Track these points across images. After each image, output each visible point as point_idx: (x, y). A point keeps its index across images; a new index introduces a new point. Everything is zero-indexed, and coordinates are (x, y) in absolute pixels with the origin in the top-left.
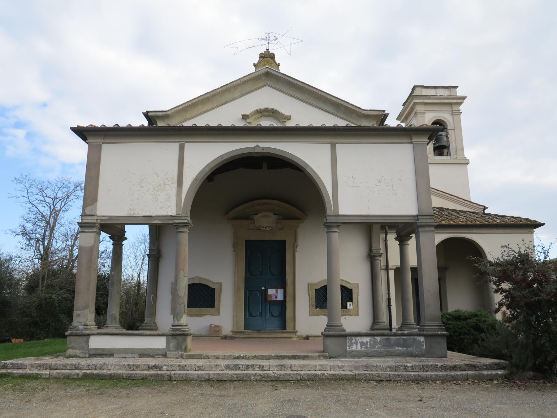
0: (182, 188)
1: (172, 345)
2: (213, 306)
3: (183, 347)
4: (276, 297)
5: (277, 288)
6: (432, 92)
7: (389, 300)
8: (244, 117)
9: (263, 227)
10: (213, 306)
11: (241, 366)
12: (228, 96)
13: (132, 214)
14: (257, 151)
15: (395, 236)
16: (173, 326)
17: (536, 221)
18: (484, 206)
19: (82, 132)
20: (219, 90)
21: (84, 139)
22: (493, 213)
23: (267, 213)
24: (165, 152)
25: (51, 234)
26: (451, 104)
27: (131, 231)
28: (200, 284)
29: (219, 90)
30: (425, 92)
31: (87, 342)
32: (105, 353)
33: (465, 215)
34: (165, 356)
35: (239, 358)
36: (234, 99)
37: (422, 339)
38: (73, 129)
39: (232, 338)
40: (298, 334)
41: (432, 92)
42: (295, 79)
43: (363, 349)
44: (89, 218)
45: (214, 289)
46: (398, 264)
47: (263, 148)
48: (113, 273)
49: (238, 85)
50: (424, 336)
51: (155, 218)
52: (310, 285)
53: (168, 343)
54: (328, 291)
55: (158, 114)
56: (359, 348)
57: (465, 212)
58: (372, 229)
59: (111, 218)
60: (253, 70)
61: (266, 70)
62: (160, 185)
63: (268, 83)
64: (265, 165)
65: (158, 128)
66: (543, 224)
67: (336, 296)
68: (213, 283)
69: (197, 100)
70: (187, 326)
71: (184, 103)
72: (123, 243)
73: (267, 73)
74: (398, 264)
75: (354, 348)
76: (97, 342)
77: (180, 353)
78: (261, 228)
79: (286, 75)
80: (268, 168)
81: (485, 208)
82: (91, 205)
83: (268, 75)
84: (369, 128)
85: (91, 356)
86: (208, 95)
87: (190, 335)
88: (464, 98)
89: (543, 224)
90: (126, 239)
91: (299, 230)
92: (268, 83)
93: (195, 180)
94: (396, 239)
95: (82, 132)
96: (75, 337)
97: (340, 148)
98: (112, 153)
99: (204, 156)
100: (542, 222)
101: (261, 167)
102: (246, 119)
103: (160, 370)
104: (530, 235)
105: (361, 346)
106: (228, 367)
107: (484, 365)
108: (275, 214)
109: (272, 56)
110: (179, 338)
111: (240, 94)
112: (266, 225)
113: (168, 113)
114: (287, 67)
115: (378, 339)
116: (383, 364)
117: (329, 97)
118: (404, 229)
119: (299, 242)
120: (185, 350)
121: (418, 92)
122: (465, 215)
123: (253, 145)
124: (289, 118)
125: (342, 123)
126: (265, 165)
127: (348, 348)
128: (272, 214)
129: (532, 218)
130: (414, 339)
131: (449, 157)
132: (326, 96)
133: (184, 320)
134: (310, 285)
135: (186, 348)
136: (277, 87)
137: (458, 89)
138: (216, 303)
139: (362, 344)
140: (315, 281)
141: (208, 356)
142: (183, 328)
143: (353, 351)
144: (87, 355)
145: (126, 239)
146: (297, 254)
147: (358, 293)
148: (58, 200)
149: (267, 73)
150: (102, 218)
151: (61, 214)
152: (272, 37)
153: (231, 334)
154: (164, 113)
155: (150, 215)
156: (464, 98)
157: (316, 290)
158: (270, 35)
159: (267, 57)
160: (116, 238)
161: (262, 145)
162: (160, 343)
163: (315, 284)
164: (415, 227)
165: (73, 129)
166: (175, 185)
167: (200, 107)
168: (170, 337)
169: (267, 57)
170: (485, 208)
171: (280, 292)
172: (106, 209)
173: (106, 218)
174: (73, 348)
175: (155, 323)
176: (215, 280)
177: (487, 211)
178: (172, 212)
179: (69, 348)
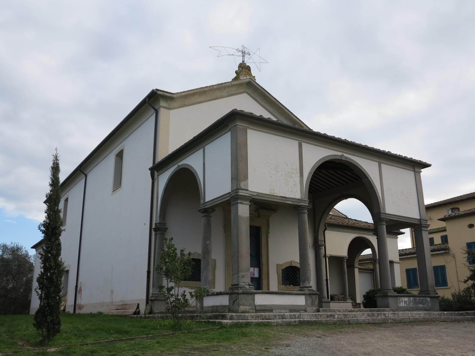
4: (254, 275)
12: (218, 93)
14: (343, 159)
20: (216, 87)
29: (216, 87)
31: (254, 300)
32: (267, 309)
36: (222, 97)
37: (429, 299)
42: (269, 94)
44: (244, 191)
47: (346, 158)
49: (228, 87)
50: (430, 297)
51: (289, 199)
52: (278, 265)
55: (166, 94)
56: (404, 305)
61: (250, 80)
62: (289, 173)
63: (248, 91)
69: (199, 90)
71: (188, 91)
79: (263, 89)
85: (257, 311)
86: (207, 89)
92: (248, 91)
93: (310, 173)
96: (244, 295)
104: (395, 238)
108: (255, 204)
110: (312, 296)
113: (175, 96)
115: (411, 298)
116: (421, 314)
117: (291, 115)
119: (271, 230)
123: (340, 154)
130: (426, 299)
132: (290, 113)
134: (278, 265)
136: (254, 96)
140: (281, 263)
141: (334, 310)
143: (401, 307)
146: (269, 239)
149: (244, 80)
152: (246, 51)
154: (171, 95)
155: (285, 196)
158: (245, 49)
159: (244, 69)
161: (346, 155)
163: (280, 265)
166: (298, 175)
167: (197, 97)
168: (308, 296)
169: (244, 69)
173: (255, 194)
174: (244, 305)
178: (298, 196)
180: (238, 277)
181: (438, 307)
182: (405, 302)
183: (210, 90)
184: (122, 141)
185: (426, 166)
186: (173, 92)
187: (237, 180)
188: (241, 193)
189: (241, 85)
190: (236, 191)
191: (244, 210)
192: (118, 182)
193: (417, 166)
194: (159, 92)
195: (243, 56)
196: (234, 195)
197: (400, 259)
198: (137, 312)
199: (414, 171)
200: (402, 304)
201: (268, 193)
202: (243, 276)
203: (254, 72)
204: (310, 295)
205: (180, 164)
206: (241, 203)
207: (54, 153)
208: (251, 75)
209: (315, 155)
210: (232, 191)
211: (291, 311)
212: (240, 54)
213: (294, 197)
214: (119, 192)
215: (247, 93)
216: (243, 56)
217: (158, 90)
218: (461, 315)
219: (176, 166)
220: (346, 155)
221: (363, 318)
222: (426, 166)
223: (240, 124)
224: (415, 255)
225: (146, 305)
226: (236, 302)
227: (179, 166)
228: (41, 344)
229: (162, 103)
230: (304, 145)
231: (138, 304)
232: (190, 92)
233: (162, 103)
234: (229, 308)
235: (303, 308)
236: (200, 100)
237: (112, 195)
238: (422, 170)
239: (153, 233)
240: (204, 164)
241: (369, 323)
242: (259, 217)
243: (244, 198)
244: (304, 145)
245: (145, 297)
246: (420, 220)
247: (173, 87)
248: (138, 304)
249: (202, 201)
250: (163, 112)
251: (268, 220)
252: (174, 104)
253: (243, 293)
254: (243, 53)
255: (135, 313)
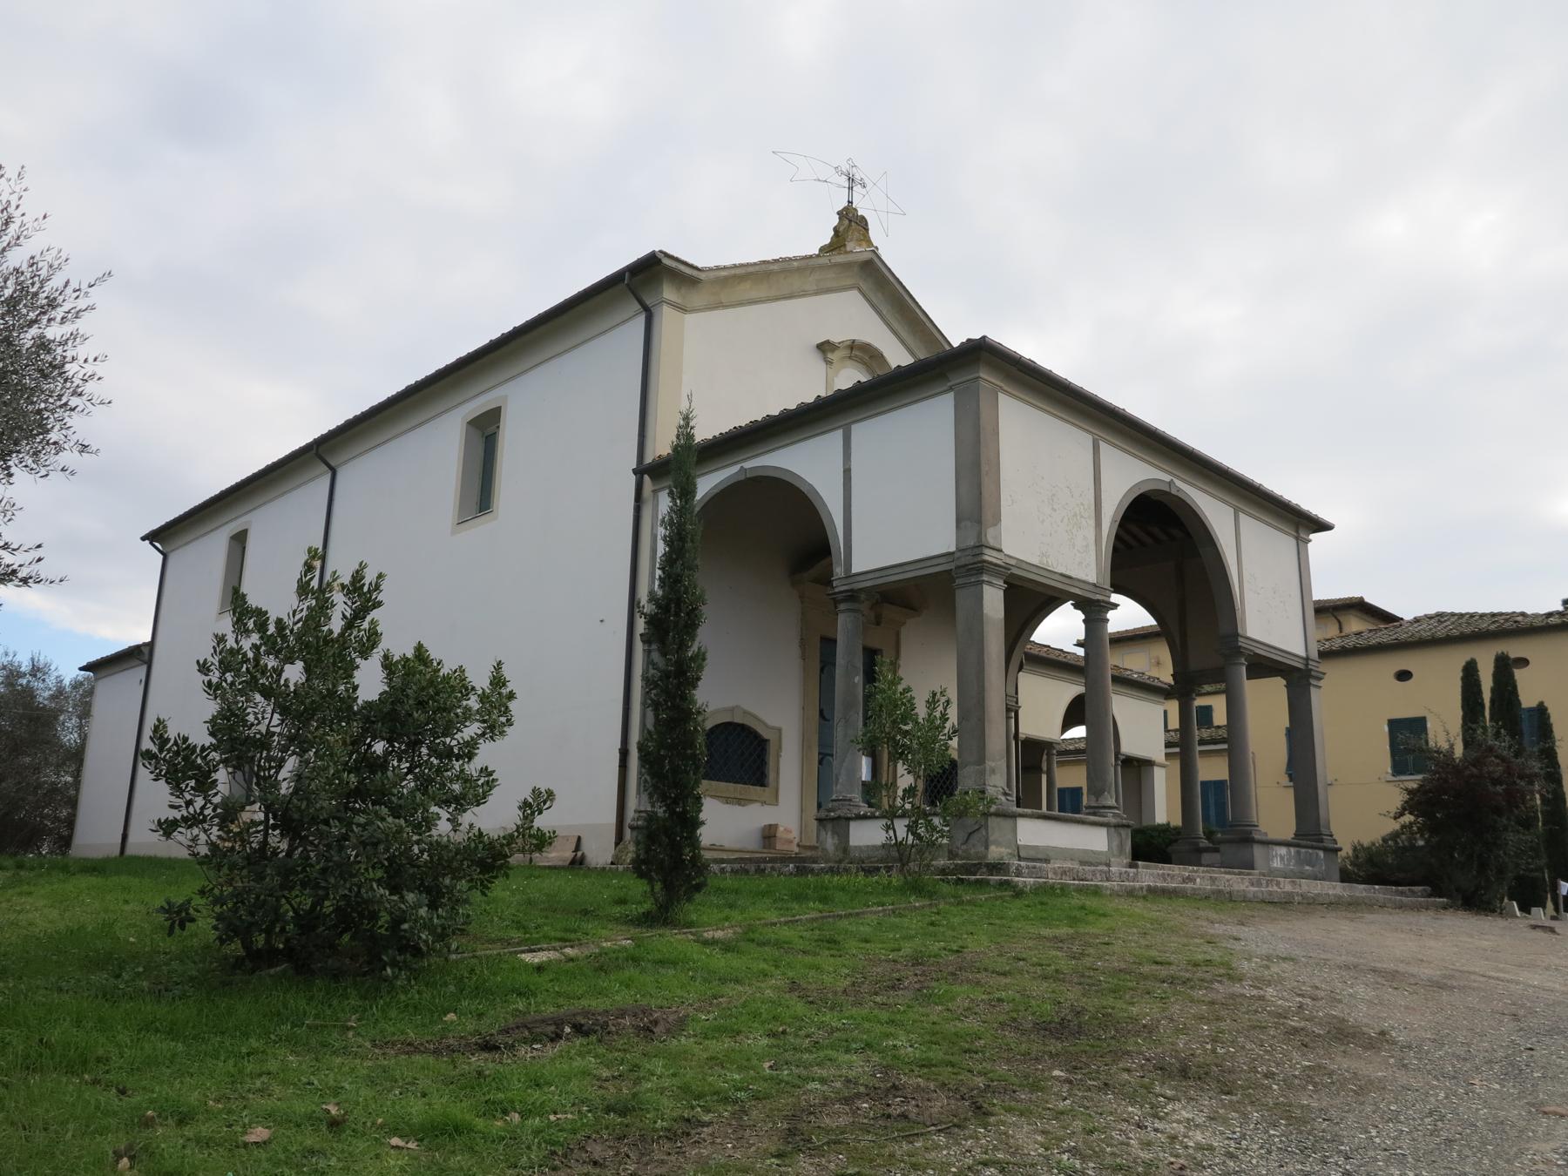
14: (1174, 492)
37: (1321, 854)
44: (994, 553)
47: (1179, 490)
55: (682, 268)
61: (870, 255)
86: (775, 267)
93: (1114, 521)
113: (702, 276)
115: (1292, 850)
123: (734, 469)
143: (1277, 869)
149: (851, 257)
152: (857, 177)
154: (695, 273)
155: (1068, 573)
159: (851, 224)
166: (1092, 522)
167: (747, 285)
169: (851, 224)
173: (1013, 562)
174: (998, 844)
180: (982, 773)
181: (1337, 875)
182: (1282, 858)
183: (783, 271)
184: (500, 384)
185: (1322, 526)
186: (696, 264)
187: (979, 522)
188: (990, 556)
189: (847, 266)
190: (977, 551)
191: (993, 600)
192: (480, 493)
193: (1303, 524)
194: (666, 261)
195: (850, 188)
196: (969, 560)
197: (1167, 755)
198: (578, 863)
199: (1297, 538)
200: (1277, 864)
201: (1035, 561)
202: (993, 771)
203: (875, 235)
204: (1117, 826)
205: (748, 465)
206: (990, 583)
207: (684, 406)
208: (869, 243)
209: (1127, 475)
210: (958, 550)
211: (1082, 863)
212: (844, 181)
213: (1084, 578)
214: (482, 528)
215: (860, 291)
216: (850, 188)
217: (666, 255)
218: (1402, 893)
219: (734, 469)
220: (1179, 483)
221: (1242, 887)
222: (1322, 526)
223: (986, 377)
224: (1225, 746)
225: (617, 844)
226: (976, 836)
227: (1171, 483)
228: (648, 920)
229: (669, 292)
230: (1103, 446)
231: (579, 838)
232: (738, 271)
233: (669, 292)
234: (950, 852)
235: (1104, 859)
236: (754, 294)
237: (453, 533)
238: (1312, 536)
239: (639, 646)
240: (847, 472)
241: (1263, 901)
242: (878, 624)
243: (996, 570)
244: (1103, 446)
245: (612, 818)
246: (1307, 659)
247: (702, 250)
248: (579, 838)
249: (839, 571)
250: (667, 318)
251: (898, 634)
252: (696, 298)
253: (997, 815)
254: (851, 180)
255: (573, 862)
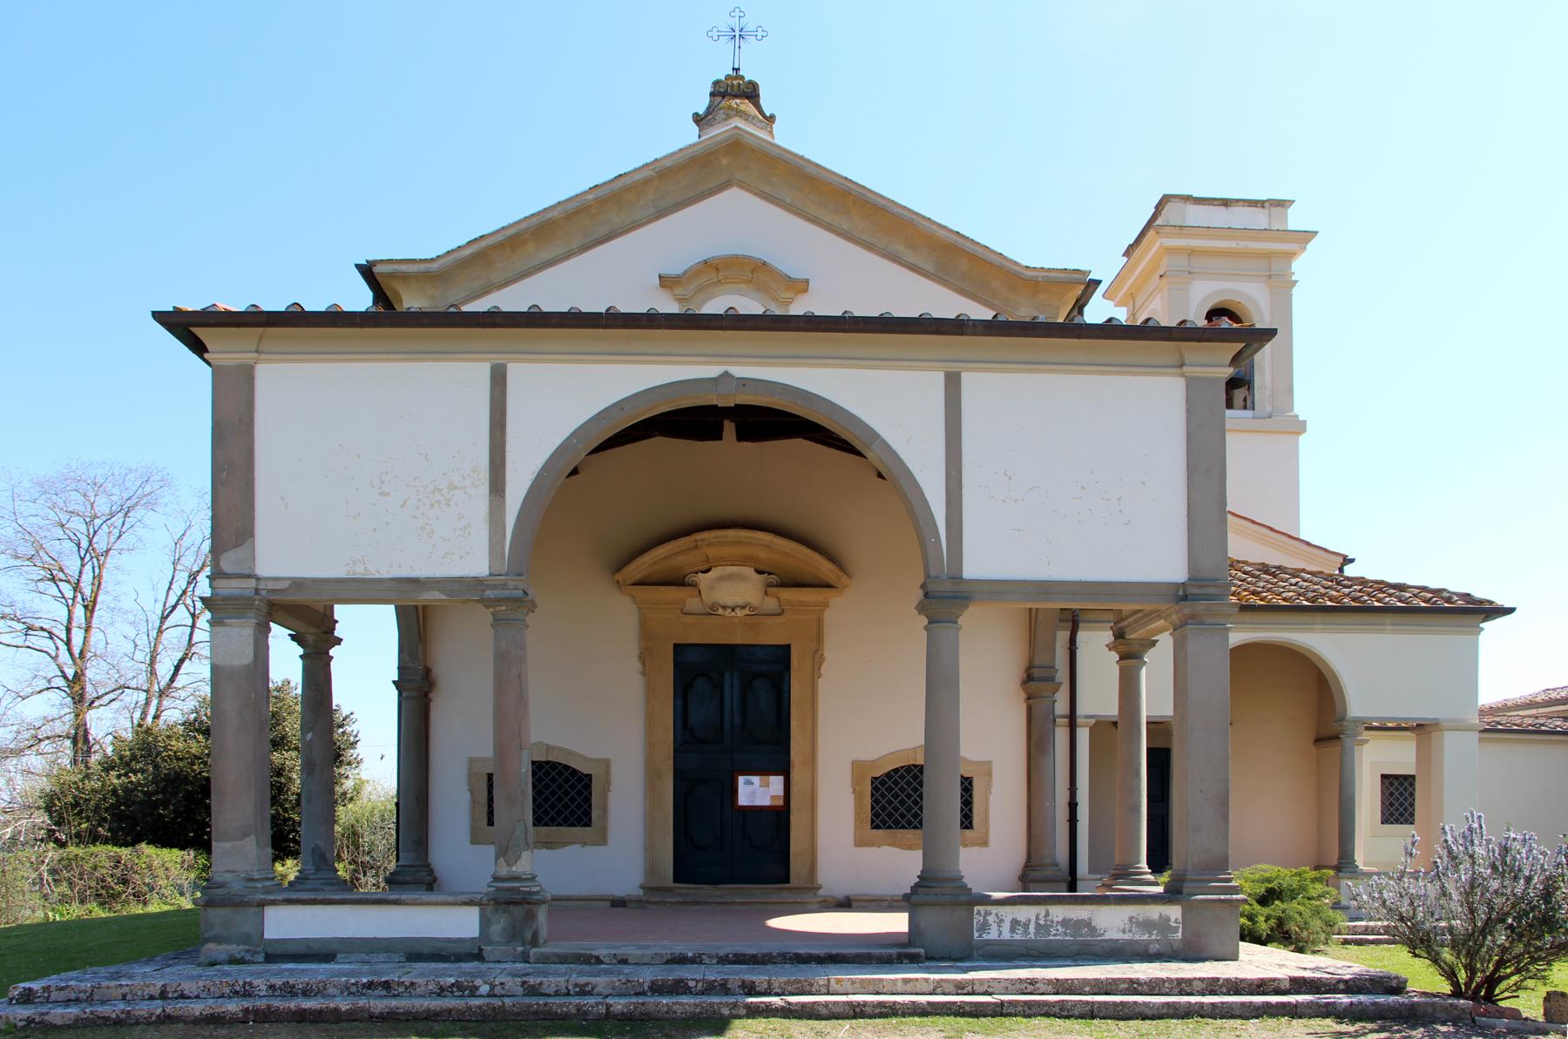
0: (503, 497)
1: (498, 927)
2: (584, 819)
3: (528, 935)
5: (764, 772)
6: (1218, 218)
7: (1073, 806)
8: (666, 282)
9: (724, 608)
10: (584, 819)
11: (692, 984)
13: (359, 571)
15: (1107, 636)
16: (496, 879)
17: (1491, 602)
18: (1345, 557)
19: (187, 327)
21: (199, 348)
22: (1371, 575)
23: (735, 569)
24: (448, 385)
25: (89, 620)
26: (1268, 256)
27: (347, 617)
28: (547, 762)
30: (1196, 216)
33: (1294, 581)
34: (479, 956)
35: (681, 960)
38: (159, 316)
39: (640, 903)
40: (821, 892)
41: (1218, 218)
43: (1017, 937)
45: (589, 777)
46: (1111, 709)
47: (744, 382)
48: (309, 736)
53: (485, 923)
54: (925, 790)
55: (404, 268)
56: (1006, 935)
57: (1295, 573)
58: (1055, 618)
59: (298, 584)
60: (689, 135)
64: (729, 428)
65: (400, 309)
66: (1510, 611)
67: (942, 801)
68: (585, 759)
70: (533, 878)
72: (332, 652)
73: (733, 143)
74: (1111, 709)
75: (993, 934)
76: (286, 923)
77: (520, 949)
78: (720, 611)
80: (740, 438)
81: (1348, 561)
82: (237, 546)
83: (736, 146)
84: (1036, 320)
85: (271, 958)
87: (543, 902)
88: (1306, 236)
89: (1510, 611)
90: (338, 641)
91: (829, 617)
94: (1111, 647)
95: (187, 327)
97: (974, 384)
98: (286, 386)
99: (564, 397)
100: (1507, 605)
101: (717, 435)
102: (670, 288)
103: (472, 995)
105: (1013, 930)
106: (657, 989)
107: (1340, 981)
108: (759, 572)
109: (751, 93)
111: (652, 210)
112: (732, 596)
114: (800, 128)
118: (1126, 615)
120: (534, 942)
121: (1171, 214)
122: (1294, 581)
124: (802, 286)
125: (946, 304)
126: (729, 428)
127: (976, 934)
128: (749, 571)
129: (1478, 594)
131: (1248, 413)
133: (526, 863)
134: (858, 767)
135: (535, 936)
137: (1291, 211)
138: (595, 814)
139: (1015, 923)
142: (524, 887)
143: (988, 942)
144: (261, 958)
145: (338, 641)
147: (989, 786)
148: (98, 522)
149: (733, 143)
150: (271, 586)
151: (111, 561)
153: (641, 892)
156: (1306, 236)
157: (874, 779)
160: (310, 639)
161: (740, 371)
162: (462, 923)
164: (1175, 617)
165: (159, 316)
169: (735, 92)
170: (1348, 561)
171: (776, 783)
172: (280, 556)
173: (285, 585)
175: (428, 865)
176: (593, 753)
177: (1350, 571)
179: (207, 941)
